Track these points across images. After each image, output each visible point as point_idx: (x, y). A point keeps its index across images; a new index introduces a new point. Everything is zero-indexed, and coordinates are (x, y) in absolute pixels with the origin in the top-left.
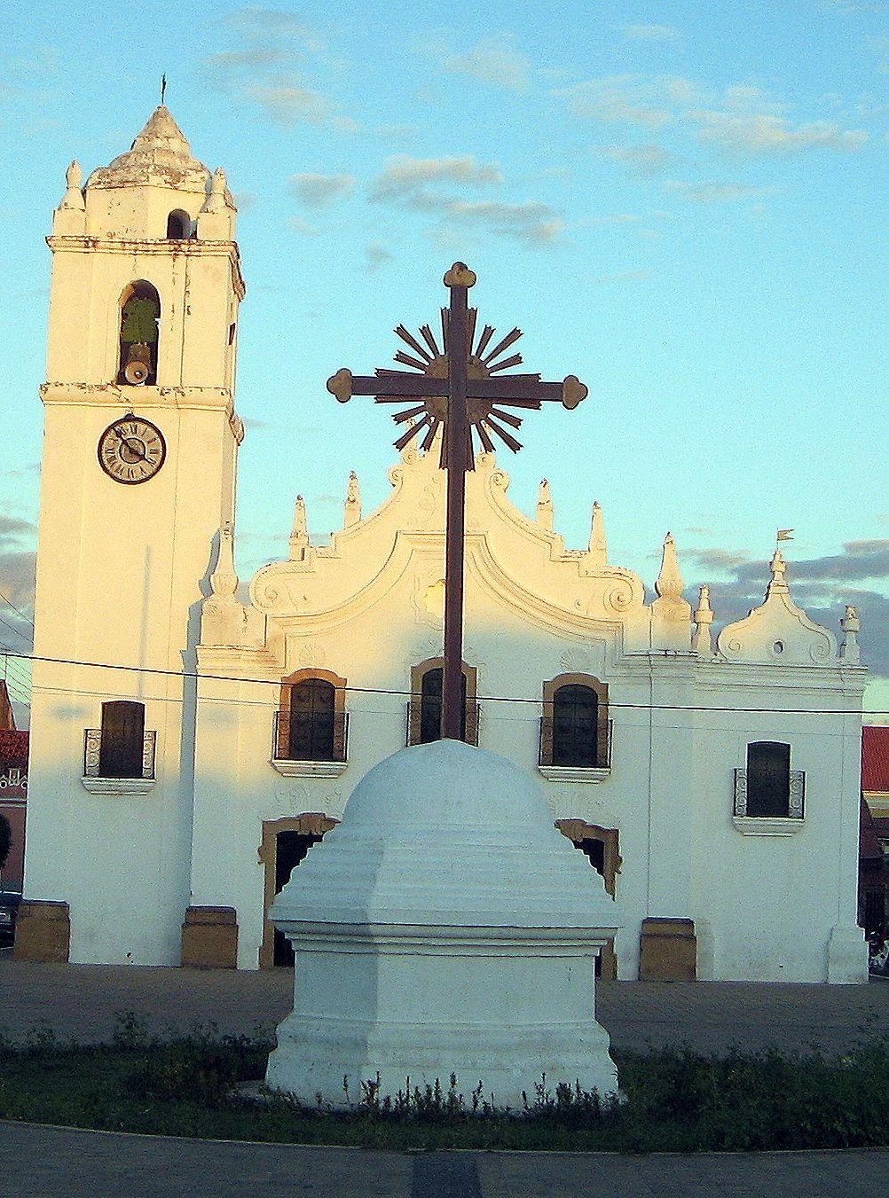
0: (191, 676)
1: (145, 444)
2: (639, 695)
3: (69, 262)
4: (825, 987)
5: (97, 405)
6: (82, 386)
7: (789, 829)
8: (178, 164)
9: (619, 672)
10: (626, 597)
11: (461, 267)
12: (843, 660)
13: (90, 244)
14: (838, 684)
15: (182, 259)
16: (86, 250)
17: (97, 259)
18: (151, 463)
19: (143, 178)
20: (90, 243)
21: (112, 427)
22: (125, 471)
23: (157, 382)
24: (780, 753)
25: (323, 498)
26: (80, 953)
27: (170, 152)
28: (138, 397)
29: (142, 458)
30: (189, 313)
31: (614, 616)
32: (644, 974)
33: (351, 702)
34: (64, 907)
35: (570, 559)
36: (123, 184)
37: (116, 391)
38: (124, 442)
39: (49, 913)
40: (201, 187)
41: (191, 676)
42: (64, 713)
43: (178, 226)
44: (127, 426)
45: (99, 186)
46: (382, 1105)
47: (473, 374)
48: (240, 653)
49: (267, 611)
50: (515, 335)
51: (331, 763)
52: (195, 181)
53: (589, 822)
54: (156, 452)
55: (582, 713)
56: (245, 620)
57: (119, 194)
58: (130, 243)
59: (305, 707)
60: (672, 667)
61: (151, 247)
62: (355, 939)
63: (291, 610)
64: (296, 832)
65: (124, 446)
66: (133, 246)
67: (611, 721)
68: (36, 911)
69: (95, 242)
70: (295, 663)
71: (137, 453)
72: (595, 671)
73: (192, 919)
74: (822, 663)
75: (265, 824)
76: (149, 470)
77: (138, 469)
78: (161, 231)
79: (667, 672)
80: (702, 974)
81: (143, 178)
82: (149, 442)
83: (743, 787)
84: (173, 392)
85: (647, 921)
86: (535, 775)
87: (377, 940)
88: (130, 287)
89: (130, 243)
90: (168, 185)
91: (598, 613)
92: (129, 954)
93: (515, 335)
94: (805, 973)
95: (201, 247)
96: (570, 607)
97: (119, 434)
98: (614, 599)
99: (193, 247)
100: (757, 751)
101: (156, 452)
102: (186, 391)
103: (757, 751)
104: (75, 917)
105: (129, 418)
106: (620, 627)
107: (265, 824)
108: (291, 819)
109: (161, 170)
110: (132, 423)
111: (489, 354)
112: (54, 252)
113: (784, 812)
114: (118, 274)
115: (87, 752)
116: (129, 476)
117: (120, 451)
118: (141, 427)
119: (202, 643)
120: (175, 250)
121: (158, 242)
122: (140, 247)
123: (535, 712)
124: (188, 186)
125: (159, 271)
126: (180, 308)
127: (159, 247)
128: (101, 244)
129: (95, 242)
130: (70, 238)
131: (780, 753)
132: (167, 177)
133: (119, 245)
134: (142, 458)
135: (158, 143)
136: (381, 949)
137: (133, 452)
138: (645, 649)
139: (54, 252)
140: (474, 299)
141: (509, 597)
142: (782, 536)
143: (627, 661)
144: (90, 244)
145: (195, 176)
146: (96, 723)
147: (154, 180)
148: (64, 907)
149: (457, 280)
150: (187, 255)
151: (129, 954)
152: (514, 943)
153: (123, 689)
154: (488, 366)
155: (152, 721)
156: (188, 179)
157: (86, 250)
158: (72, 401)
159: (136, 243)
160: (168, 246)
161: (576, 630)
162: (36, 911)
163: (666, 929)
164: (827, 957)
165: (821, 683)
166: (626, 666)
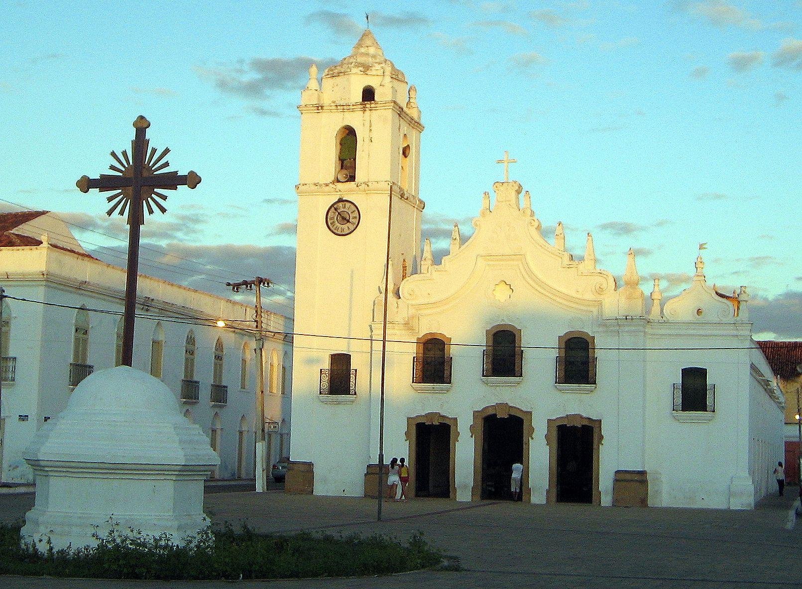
0: (384, 341)
2: (612, 342)
3: (309, 118)
4: (728, 511)
5: (328, 193)
6: (316, 185)
7: (706, 418)
8: (370, 60)
9: (601, 329)
10: (604, 286)
11: (142, 118)
12: (738, 318)
13: (320, 108)
14: (735, 332)
16: (318, 111)
17: (324, 116)
18: (353, 224)
20: (320, 107)
21: (333, 205)
22: (340, 229)
23: (356, 180)
24: (701, 373)
25: (763, 237)
26: (319, 489)
27: (367, 54)
28: (346, 190)
29: (348, 221)
31: (599, 298)
32: (616, 502)
33: (453, 351)
34: (310, 465)
37: (333, 186)
38: (339, 213)
39: (302, 468)
40: (380, 72)
41: (384, 341)
42: (310, 361)
43: (368, 94)
44: (341, 204)
45: (328, 76)
46: (31, 549)
47: (145, 174)
48: (394, 325)
49: (408, 302)
50: (113, 154)
51: (569, 385)
52: (377, 69)
53: (584, 415)
54: (355, 218)
55: (580, 354)
57: (337, 80)
59: (431, 354)
60: (630, 325)
61: (351, 107)
62: (70, 470)
64: (424, 423)
65: (339, 216)
66: (342, 107)
67: (596, 358)
68: (295, 467)
69: (322, 107)
70: (425, 328)
72: (589, 330)
73: (620, 476)
74: (725, 320)
75: (408, 419)
77: (346, 227)
78: (360, 99)
79: (627, 329)
80: (650, 503)
82: (352, 213)
83: (679, 394)
84: (363, 185)
85: (617, 472)
87: (47, 469)
88: (344, 130)
90: (362, 73)
91: (589, 296)
92: (344, 491)
93: (113, 154)
94: (716, 502)
95: (377, 105)
96: (574, 294)
97: (336, 209)
98: (597, 287)
99: (372, 106)
100: (688, 373)
101: (355, 218)
102: (370, 184)
103: (688, 373)
104: (316, 470)
106: (600, 304)
107: (408, 419)
108: (421, 416)
109: (358, 65)
111: (118, 163)
112: (302, 114)
113: (704, 408)
114: (334, 123)
115: (354, 382)
117: (337, 218)
118: (348, 205)
119: (375, 320)
121: (354, 104)
122: (345, 107)
123: (555, 354)
124: (374, 73)
125: (355, 120)
126: (367, 140)
128: (324, 108)
129: (322, 107)
131: (701, 373)
132: (361, 69)
133: (335, 108)
134: (348, 221)
135: (363, 50)
136: (50, 474)
137: (344, 218)
138: (615, 315)
139: (302, 114)
140: (149, 134)
141: (539, 289)
142: (701, 247)
143: (605, 323)
144: (320, 108)
145: (378, 67)
146: (326, 365)
147: (354, 70)
148: (310, 465)
149: (139, 125)
150: (370, 110)
151: (344, 491)
152: (107, 471)
153: (341, 348)
154: (153, 169)
156: (373, 68)
157: (318, 111)
158: (311, 193)
159: (343, 106)
161: (574, 305)
162: (295, 467)
163: (628, 477)
164: (731, 494)
165: (725, 332)
166: (605, 325)
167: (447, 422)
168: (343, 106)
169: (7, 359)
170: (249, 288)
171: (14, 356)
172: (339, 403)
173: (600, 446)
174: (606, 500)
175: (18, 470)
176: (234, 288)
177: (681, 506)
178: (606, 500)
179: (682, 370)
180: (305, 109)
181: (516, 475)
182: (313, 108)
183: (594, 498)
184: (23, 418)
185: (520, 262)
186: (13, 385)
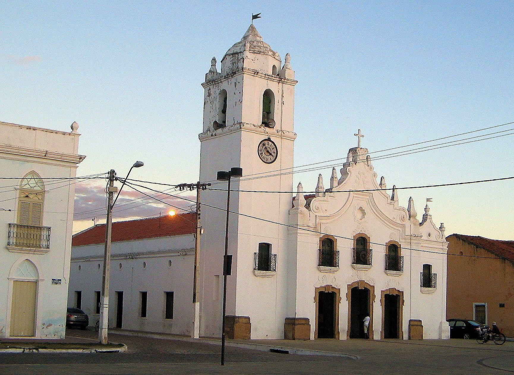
1: (271, 149)
5: (257, 132)
6: (254, 125)
10: (405, 216)
15: (281, 84)
16: (254, 75)
17: (257, 79)
19: (267, 52)
26: (254, 335)
30: (283, 104)
35: (392, 203)
36: (259, 53)
39: (244, 321)
44: (266, 142)
56: (310, 217)
58: (268, 75)
63: (322, 214)
66: (268, 77)
71: (269, 153)
76: (273, 159)
81: (267, 52)
85: (410, 321)
86: (317, 272)
89: (268, 75)
92: (267, 335)
105: (269, 139)
110: (267, 141)
116: (267, 161)
118: (270, 143)
120: (280, 80)
125: (274, 87)
126: (280, 102)
127: (275, 78)
128: (259, 74)
130: (250, 70)
137: (268, 152)
142: (428, 200)
148: (248, 318)
151: (267, 335)
155: (274, 251)
157: (254, 75)
160: (278, 78)
162: (241, 320)
167: (334, 291)
168: (269, 76)
169: (40, 228)
170: (192, 189)
171: (49, 226)
172: (265, 276)
173: (340, 304)
174: (406, 336)
175: (51, 328)
176: (180, 188)
177: (259, 338)
178: (406, 336)
179: (423, 265)
180: (248, 71)
181: (367, 323)
182: (252, 72)
183: (400, 335)
184: (56, 282)
185: (368, 198)
186: (47, 252)
